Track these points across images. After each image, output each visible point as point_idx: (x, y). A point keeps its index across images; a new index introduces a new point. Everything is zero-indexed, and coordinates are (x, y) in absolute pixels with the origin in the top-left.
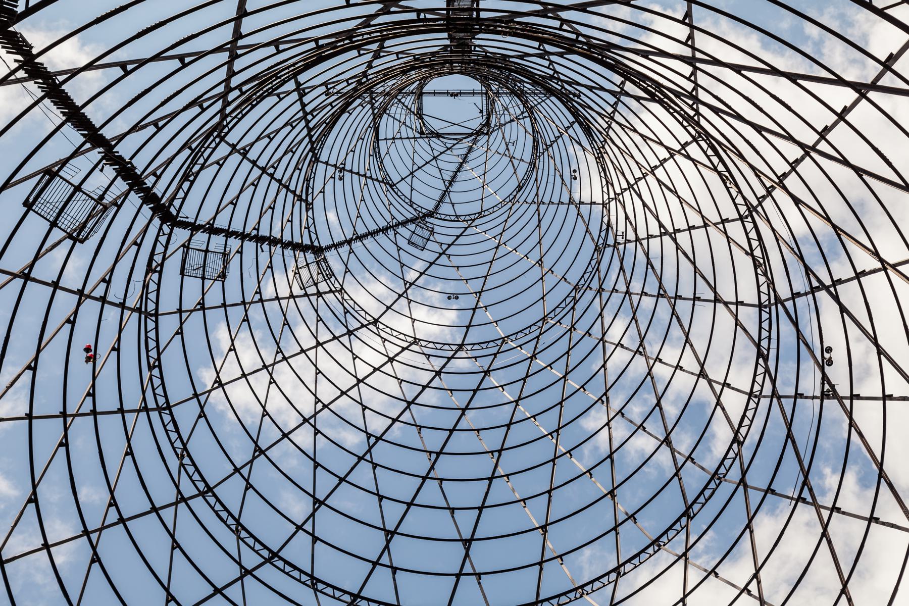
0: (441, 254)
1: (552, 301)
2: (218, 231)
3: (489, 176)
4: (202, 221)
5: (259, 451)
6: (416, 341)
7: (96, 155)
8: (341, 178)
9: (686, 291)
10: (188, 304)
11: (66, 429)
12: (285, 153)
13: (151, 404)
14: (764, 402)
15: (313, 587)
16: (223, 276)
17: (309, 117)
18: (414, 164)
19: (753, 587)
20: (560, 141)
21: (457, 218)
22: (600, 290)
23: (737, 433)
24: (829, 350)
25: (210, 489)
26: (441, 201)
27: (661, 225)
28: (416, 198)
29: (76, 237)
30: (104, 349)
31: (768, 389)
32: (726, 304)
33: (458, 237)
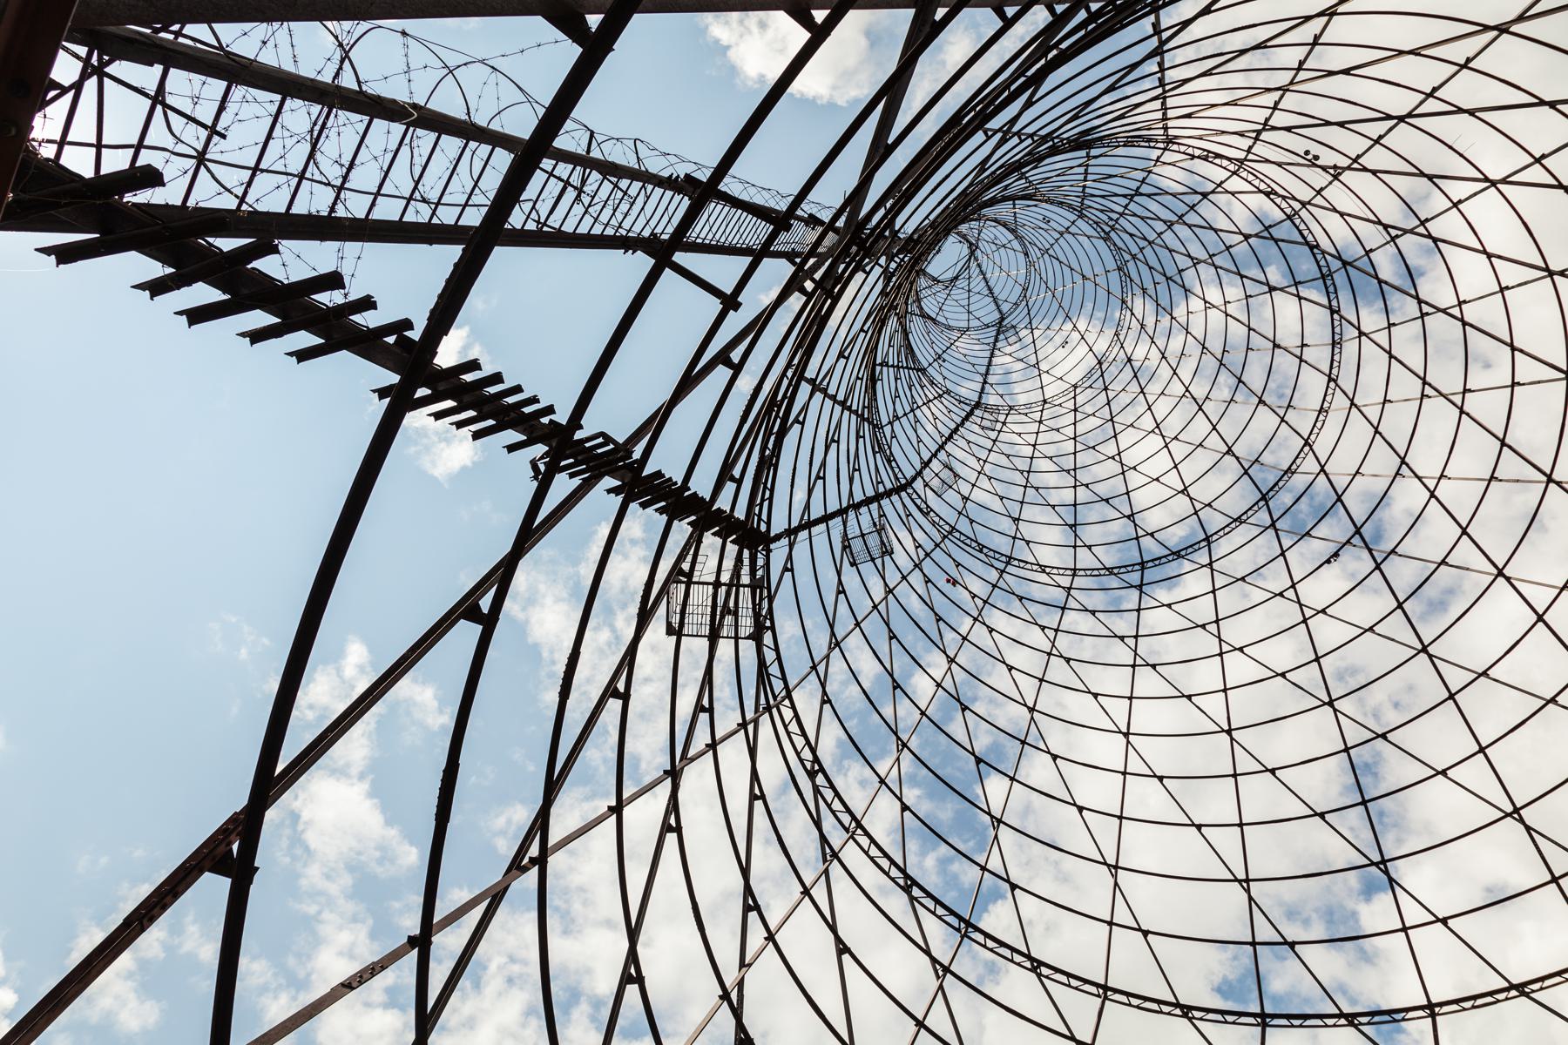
1: (1116, 288)
2: (930, 460)
4: (918, 467)
6: (1075, 386)
7: (852, 514)
9: (1182, 209)
10: (959, 506)
14: (1303, 213)
16: (956, 475)
19: (1426, 309)
22: (1134, 257)
23: (1307, 243)
24: (1307, 153)
26: (998, 307)
27: (1125, 196)
28: (986, 320)
29: (887, 552)
30: (954, 573)
31: (1297, 206)
32: (1213, 192)
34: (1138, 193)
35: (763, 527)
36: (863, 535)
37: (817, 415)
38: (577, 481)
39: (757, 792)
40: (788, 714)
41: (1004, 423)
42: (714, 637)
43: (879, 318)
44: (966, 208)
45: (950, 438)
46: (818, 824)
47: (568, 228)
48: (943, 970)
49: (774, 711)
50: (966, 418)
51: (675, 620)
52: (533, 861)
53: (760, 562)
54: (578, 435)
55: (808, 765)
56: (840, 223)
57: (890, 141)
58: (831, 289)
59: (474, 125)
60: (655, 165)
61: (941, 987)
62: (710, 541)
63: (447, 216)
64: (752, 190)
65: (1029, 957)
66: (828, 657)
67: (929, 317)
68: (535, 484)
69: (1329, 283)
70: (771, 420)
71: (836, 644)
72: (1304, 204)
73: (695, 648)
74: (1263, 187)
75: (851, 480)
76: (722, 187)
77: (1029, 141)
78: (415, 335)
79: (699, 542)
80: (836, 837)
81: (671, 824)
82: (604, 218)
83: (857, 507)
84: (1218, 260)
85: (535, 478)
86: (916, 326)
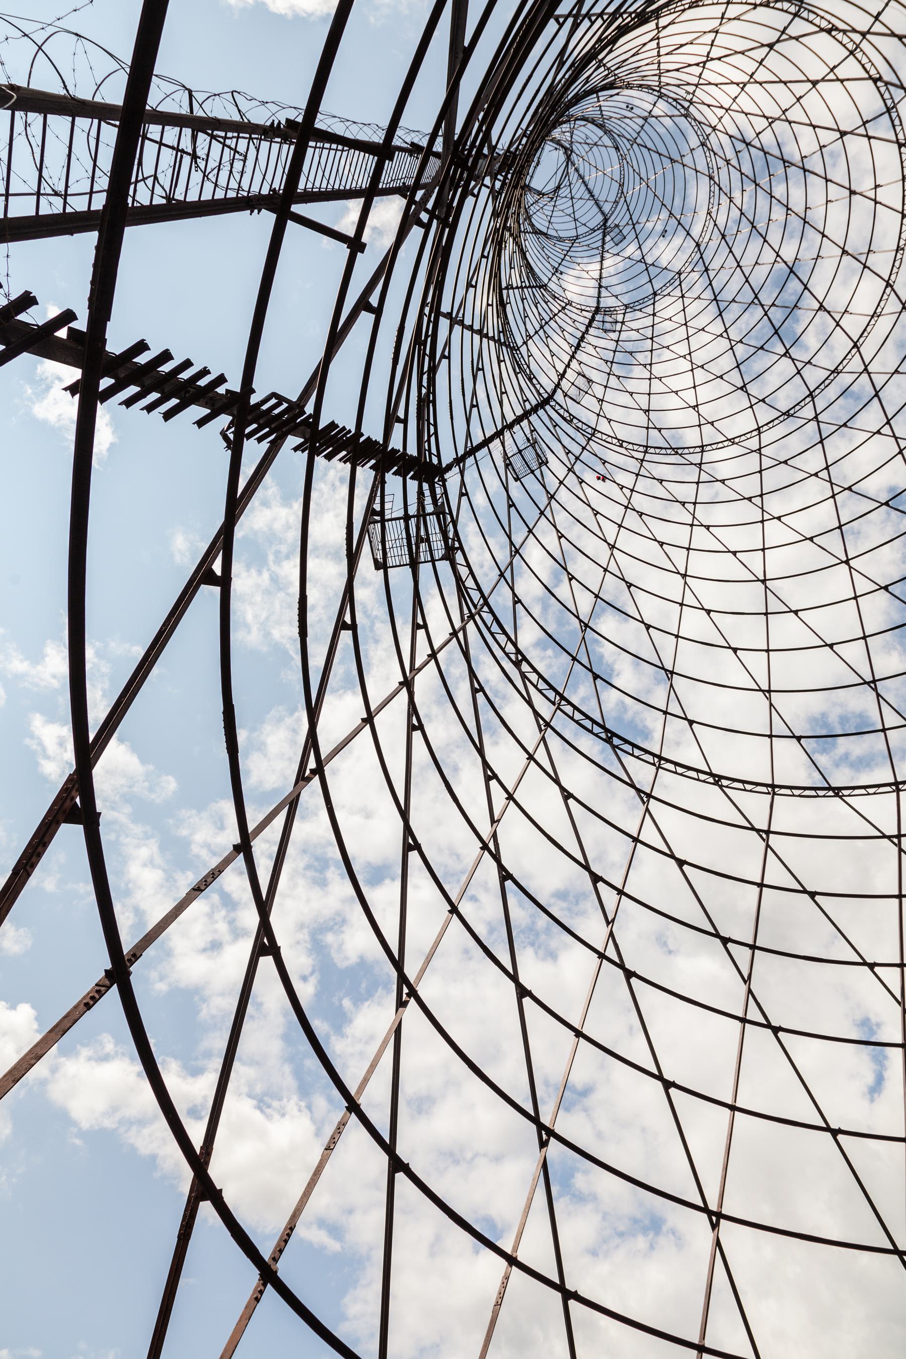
0: (634, 228)
2: (565, 372)
3: (601, 166)
5: (695, 407)
7: (507, 434)
8: (561, 273)
11: (634, 510)
12: (537, 308)
13: (641, 456)
15: (789, 416)
16: (590, 381)
17: (524, 285)
18: (569, 215)
20: (603, 108)
21: (616, 202)
23: (870, 78)
25: (702, 446)
26: (600, 208)
27: (697, 65)
28: (592, 225)
29: (543, 463)
30: (600, 468)
31: (857, 38)
32: (778, 41)
33: (628, 209)
34: (709, 58)
35: (435, 461)
36: (520, 452)
37: (459, 345)
38: (265, 445)
39: (476, 686)
40: (488, 618)
41: (623, 323)
42: (414, 564)
43: (497, 240)
44: (553, 110)
45: (578, 347)
46: (530, 703)
47: (192, 197)
48: (645, 796)
49: (477, 617)
50: (589, 325)
51: (379, 556)
52: (313, 772)
53: (439, 491)
54: (254, 399)
55: (513, 657)
56: (438, 147)
57: (466, 44)
58: (447, 217)
59: (73, 99)
60: (260, 117)
61: (647, 810)
62: (393, 482)
63: (79, 205)
64: (354, 128)
65: (711, 774)
66: (511, 563)
67: (542, 233)
68: (230, 452)
69: (894, 115)
70: (422, 354)
71: (516, 551)
72: (863, 35)
73: (401, 577)
74: (824, 24)
75: (501, 403)
76: (319, 125)
77: (600, 22)
78: (81, 324)
79: (383, 482)
80: (546, 709)
81: (415, 724)
82: (222, 181)
83: (510, 427)
84: (790, 115)
85: (228, 447)
86: (530, 243)
